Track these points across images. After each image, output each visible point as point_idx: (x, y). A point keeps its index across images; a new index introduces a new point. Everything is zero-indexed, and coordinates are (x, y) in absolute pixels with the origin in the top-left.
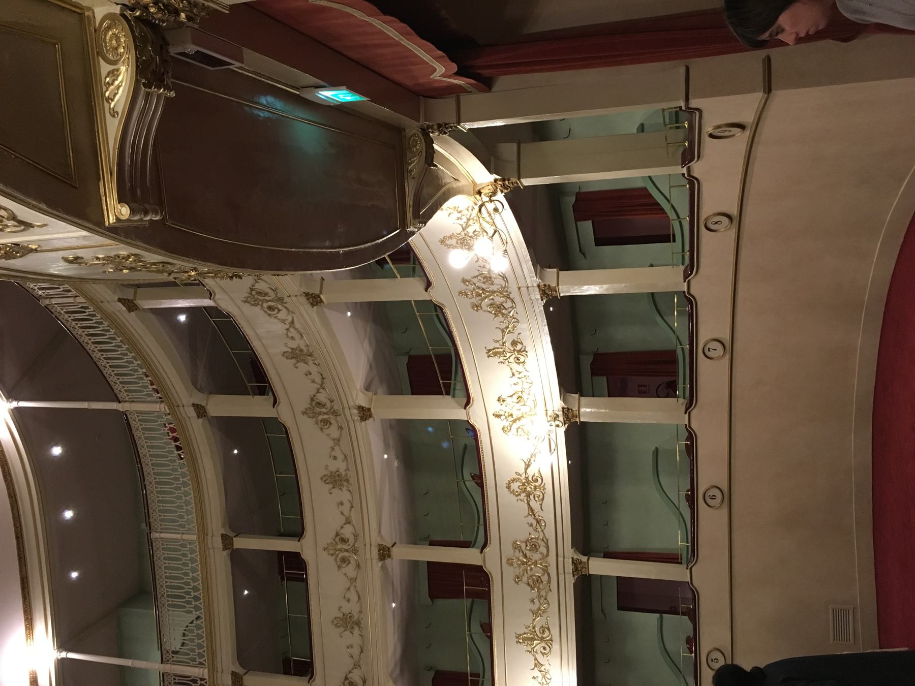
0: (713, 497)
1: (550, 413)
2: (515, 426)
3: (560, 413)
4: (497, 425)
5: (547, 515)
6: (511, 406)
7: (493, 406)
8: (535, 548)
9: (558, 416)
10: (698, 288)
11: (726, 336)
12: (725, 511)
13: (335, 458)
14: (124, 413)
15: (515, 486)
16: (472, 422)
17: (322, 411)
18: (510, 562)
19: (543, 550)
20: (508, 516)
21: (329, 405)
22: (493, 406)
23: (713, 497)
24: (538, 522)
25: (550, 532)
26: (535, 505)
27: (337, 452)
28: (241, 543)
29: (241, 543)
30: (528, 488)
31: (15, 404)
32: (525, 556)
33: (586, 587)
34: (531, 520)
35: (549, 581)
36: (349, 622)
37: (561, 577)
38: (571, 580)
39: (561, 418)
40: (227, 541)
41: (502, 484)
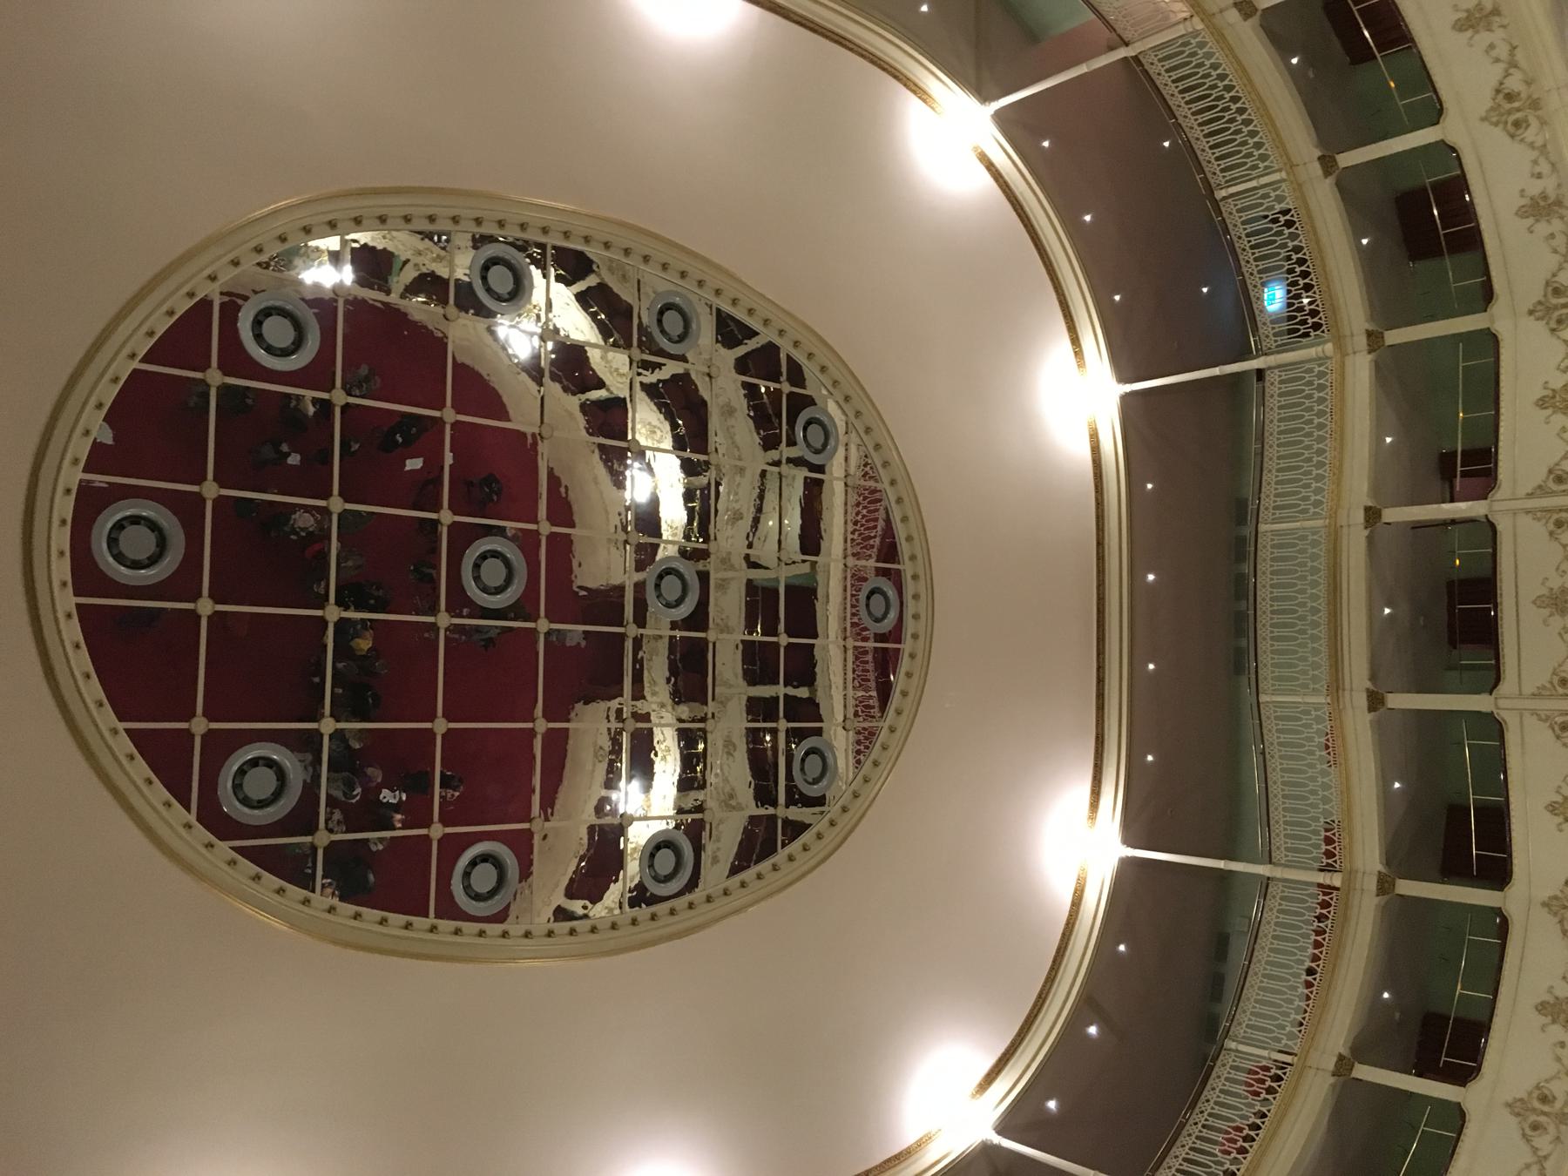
14: (1136, 58)
28: (1347, 159)
29: (1347, 159)
40: (1328, 164)
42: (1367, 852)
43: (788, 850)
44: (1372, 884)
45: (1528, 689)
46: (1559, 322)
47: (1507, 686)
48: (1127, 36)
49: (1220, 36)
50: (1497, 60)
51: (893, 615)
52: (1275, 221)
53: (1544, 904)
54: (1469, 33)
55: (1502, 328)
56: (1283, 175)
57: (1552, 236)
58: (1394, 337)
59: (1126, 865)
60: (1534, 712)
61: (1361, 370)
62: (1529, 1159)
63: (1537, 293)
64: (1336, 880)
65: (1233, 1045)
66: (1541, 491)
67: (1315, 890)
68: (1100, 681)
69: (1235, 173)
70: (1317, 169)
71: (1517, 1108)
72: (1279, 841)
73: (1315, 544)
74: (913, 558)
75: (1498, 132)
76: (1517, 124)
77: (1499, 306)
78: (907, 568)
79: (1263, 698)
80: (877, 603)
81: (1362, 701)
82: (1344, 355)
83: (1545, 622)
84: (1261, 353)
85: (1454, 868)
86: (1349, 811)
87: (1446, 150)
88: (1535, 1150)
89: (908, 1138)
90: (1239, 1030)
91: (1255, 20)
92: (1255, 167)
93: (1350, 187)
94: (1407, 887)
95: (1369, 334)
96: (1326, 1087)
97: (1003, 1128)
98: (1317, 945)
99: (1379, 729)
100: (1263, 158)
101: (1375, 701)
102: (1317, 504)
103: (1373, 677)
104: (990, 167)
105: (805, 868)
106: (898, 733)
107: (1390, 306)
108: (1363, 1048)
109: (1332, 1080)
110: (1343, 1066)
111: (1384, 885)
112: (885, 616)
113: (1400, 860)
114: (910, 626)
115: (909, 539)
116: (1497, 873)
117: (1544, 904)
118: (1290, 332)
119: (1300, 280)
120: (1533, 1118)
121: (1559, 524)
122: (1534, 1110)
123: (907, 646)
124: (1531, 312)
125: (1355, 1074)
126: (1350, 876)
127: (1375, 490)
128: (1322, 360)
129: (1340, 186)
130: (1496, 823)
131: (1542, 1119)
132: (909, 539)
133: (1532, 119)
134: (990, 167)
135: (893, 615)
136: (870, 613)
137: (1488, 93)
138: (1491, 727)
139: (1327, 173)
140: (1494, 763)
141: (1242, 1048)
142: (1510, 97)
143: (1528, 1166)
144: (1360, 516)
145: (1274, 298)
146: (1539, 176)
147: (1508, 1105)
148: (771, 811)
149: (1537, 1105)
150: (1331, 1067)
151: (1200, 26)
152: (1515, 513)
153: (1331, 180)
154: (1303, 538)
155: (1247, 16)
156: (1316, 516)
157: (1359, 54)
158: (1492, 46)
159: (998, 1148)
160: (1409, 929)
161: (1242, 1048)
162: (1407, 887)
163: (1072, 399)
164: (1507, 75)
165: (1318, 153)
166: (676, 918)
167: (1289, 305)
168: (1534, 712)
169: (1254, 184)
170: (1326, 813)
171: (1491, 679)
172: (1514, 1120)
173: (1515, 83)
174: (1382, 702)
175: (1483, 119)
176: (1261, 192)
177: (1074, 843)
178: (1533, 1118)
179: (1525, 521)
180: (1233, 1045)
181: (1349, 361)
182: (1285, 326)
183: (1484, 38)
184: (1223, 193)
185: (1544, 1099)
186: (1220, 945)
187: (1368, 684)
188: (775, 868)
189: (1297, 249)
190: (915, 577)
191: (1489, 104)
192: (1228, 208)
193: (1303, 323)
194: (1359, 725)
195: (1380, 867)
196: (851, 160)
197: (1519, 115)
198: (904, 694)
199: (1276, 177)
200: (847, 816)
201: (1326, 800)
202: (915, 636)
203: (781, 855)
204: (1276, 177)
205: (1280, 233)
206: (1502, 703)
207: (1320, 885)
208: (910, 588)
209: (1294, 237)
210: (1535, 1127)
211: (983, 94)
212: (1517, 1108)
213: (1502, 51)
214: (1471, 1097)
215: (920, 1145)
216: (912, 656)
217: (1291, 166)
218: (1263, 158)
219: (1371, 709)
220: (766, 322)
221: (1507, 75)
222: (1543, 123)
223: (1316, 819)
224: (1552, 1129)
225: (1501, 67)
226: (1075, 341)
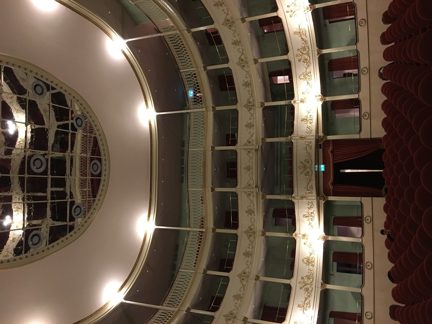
0: (368, 220)
1: (305, 7)
2: (294, 14)
3: (309, 7)
4: (288, 15)
5: (308, 39)
6: (292, 8)
7: (286, 9)
8: (308, 162)
9: (308, 8)
10: (364, 293)
11: (368, 66)
12: (366, 27)
13: (235, 36)
14: (163, 36)
15: (305, 260)
16: (279, 16)
17: (229, 23)
18: (297, 56)
19: (307, 49)
20: (294, 42)
21: (231, 20)
22: (286, 9)
23: (368, 220)
24: (305, 42)
25: (309, 44)
26: (304, 37)
27: (236, 35)
28: (209, 68)
29: (209, 68)
30: (309, 261)
31: (127, 41)
32: (302, 53)
33: (322, 59)
34: (303, 42)
35: (310, 59)
36: (247, 84)
37: (313, 52)
38: (317, 57)
39: (309, 9)
40: (205, 68)
41: (301, 259)
42: (210, 223)
43: (70, 234)
44: (211, 230)
45: (243, 187)
46: (250, 109)
47: (239, 186)
48: (161, 31)
49: (182, 35)
50: (240, 52)
51: (99, 170)
52: (193, 76)
53: (245, 232)
54: (235, 45)
55: (239, 109)
56: (195, 69)
57: (249, 91)
58: (218, 108)
59: (156, 230)
60: (244, 192)
61: (211, 115)
62: (242, 286)
63: (245, 102)
64: (204, 230)
65: (181, 270)
66: (245, 145)
67: (198, 233)
68: (151, 185)
69: (185, 67)
70: (203, 69)
71: (239, 276)
72: (191, 222)
73: (201, 154)
74: (105, 155)
75: (239, 67)
76: (243, 66)
77: (239, 104)
78: (103, 157)
79: (189, 189)
80: (95, 167)
81: (210, 189)
82: (207, 111)
83: (245, 89)
84: (189, 109)
85: (227, 226)
86: (207, 214)
87: (229, 69)
88: (243, 284)
89: (104, 303)
90: (182, 267)
91: (191, 34)
92: (189, 66)
93: (209, 73)
94: (218, 231)
95: (213, 107)
96: (201, 277)
97: (126, 299)
98: (199, 245)
99: (213, 196)
100: (191, 64)
101: (213, 190)
102: (201, 145)
103: (212, 184)
104: (125, 55)
105: (75, 238)
106: (100, 201)
107: (217, 102)
108: (209, 267)
109: (202, 275)
110: (205, 271)
111: (214, 230)
112: (97, 170)
113: (217, 225)
114: (103, 173)
115: (104, 150)
116: (236, 226)
117: (245, 232)
118: (194, 102)
119: (197, 90)
120: (242, 277)
121: (249, 152)
122: (242, 276)
123: (103, 178)
124: (245, 106)
125: (207, 273)
126: (207, 229)
127: (213, 143)
128: (203, 112)
129: (207, 73)
130: (236, 215)
131: (244, 277)
132: (104, 150)
133: (246, 66)
134: (125, 55)
135: (99, 170)
136: (93, 170)
137: (238, 59)
138: (235, 195)
139: (205, 70)
140: (235, 203)
141: (183, 270)
142: (242, 60)
143: (241, 288)
144: (210, 148)
145: (191, 93)
146: (247, 78)
147: (237, 275)
148: (65, 223)
149: (243, 275)
150: (202, 272)
151: (178, 32)
152: (241, 149)
153: (205, 72)
154: (198, 152)
155: (189, 33)
156: (201, 148)
157: (212, 44)
158: (239, 49)
159: (125, 303)
160: (219, 239)
161: (183, 270)
162: (218, 231)
163: (145, 115)
164: (247, 268)
165: (203, 65)
166: (39, 255)
167: (194, 95)
168: (244, 192)
169: (189, 70)
170: (202, 215)
171: (235, 185)
172: (239, 278)
173: (243, 57)
174: (214, 190)
175: (237, 64)
176: (191, 72)
177: (144, 226)
178: (242, 277)
179: (243, 151)
180: (181, 270)
181: (208, 113)
182: (193, 100)
183: (237, 47)
184: (182, 71)
185: (244, 273)
186: (177, 248)
187: (211, 186)
188: (67, 239)
189: (197, 83)
190: (105, 160)
191: (238, 61)
192: (183, 74)
193: (197, 100)
194: (209, 195)
195: (213, 227)
196: (90, 50)
197: (243, 64)
198: (102, 190)
199: (194, 69)
200: (87, 223)
201: (202, 212)
202: (105, 175)
203: (68, 235)
204: (194, 69)
205: (193, 79)
206: (238, 190)
207: (200, 231)
208: (104, 162)
209: (196, 80)
210: (243, 279)
211: (124, 37)
212: (239, 276)
213: (241, 50)
214: (230, 275)
215: (107, 304)
216: (104, 180)
217: (197, 67)
218: (191, 64)
219: (212, 191)
220: (90, 117)
221: (247, 268)
222: (248, 66)
223: (199, 217)
224: (246, 279)
225: (240, 54)
226: (147, 104)
